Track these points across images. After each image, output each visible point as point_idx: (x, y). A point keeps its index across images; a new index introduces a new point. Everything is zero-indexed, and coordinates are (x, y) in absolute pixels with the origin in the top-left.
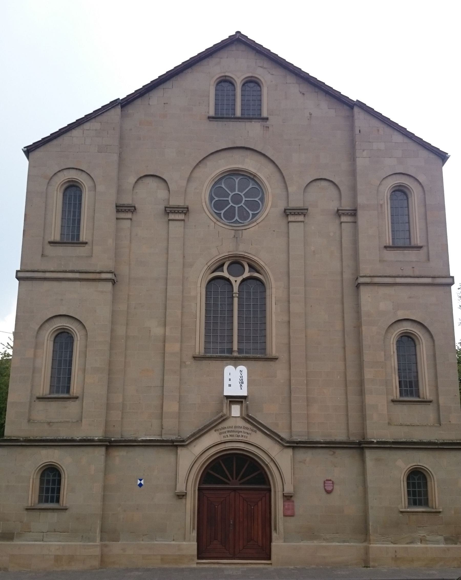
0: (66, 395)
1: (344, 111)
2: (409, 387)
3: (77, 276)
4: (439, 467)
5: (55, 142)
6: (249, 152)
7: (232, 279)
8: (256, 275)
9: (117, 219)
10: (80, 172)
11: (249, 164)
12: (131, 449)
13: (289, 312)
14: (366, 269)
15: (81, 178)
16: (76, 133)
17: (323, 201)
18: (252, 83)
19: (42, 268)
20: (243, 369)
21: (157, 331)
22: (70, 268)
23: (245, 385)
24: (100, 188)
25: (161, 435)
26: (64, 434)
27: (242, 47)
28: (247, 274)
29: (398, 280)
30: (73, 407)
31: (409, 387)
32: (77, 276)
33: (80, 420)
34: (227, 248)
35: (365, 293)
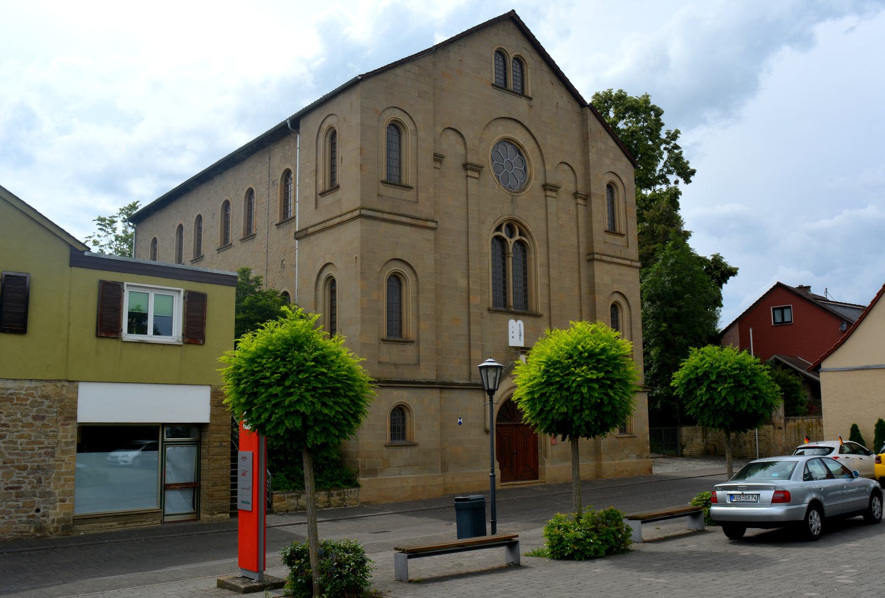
0: (398, 339)
1: (577, 107)
2: (395, 333)
3: (409, 220)
4: (1, 464)
5: (382, 76)
6: (518, 125)
7: (508, 239)
8: (524, 238)
9: (546, 196)
10: (403, 113)
11: (520, 136)
12: (451, 391)
13: (549, 277)
14: (598, 247)
15: (405, 119)
16: (399, 71)
17: (567, 182)
18: (519, 60)
19: (379, 208)
20: (520, 322)
21: (463, 283)
22: (401, 212)
23: (522, 337)
24: (421, 134)
25: (470, 378)
26: (408, 375)
27: (512, 25)
28: (517, 237)
29: (615, 260)
30: (410, 350)
31: (395, 333)
32: (409, 220)
33: (418, 364)
34: (504, 212)
35: (597, 266)
